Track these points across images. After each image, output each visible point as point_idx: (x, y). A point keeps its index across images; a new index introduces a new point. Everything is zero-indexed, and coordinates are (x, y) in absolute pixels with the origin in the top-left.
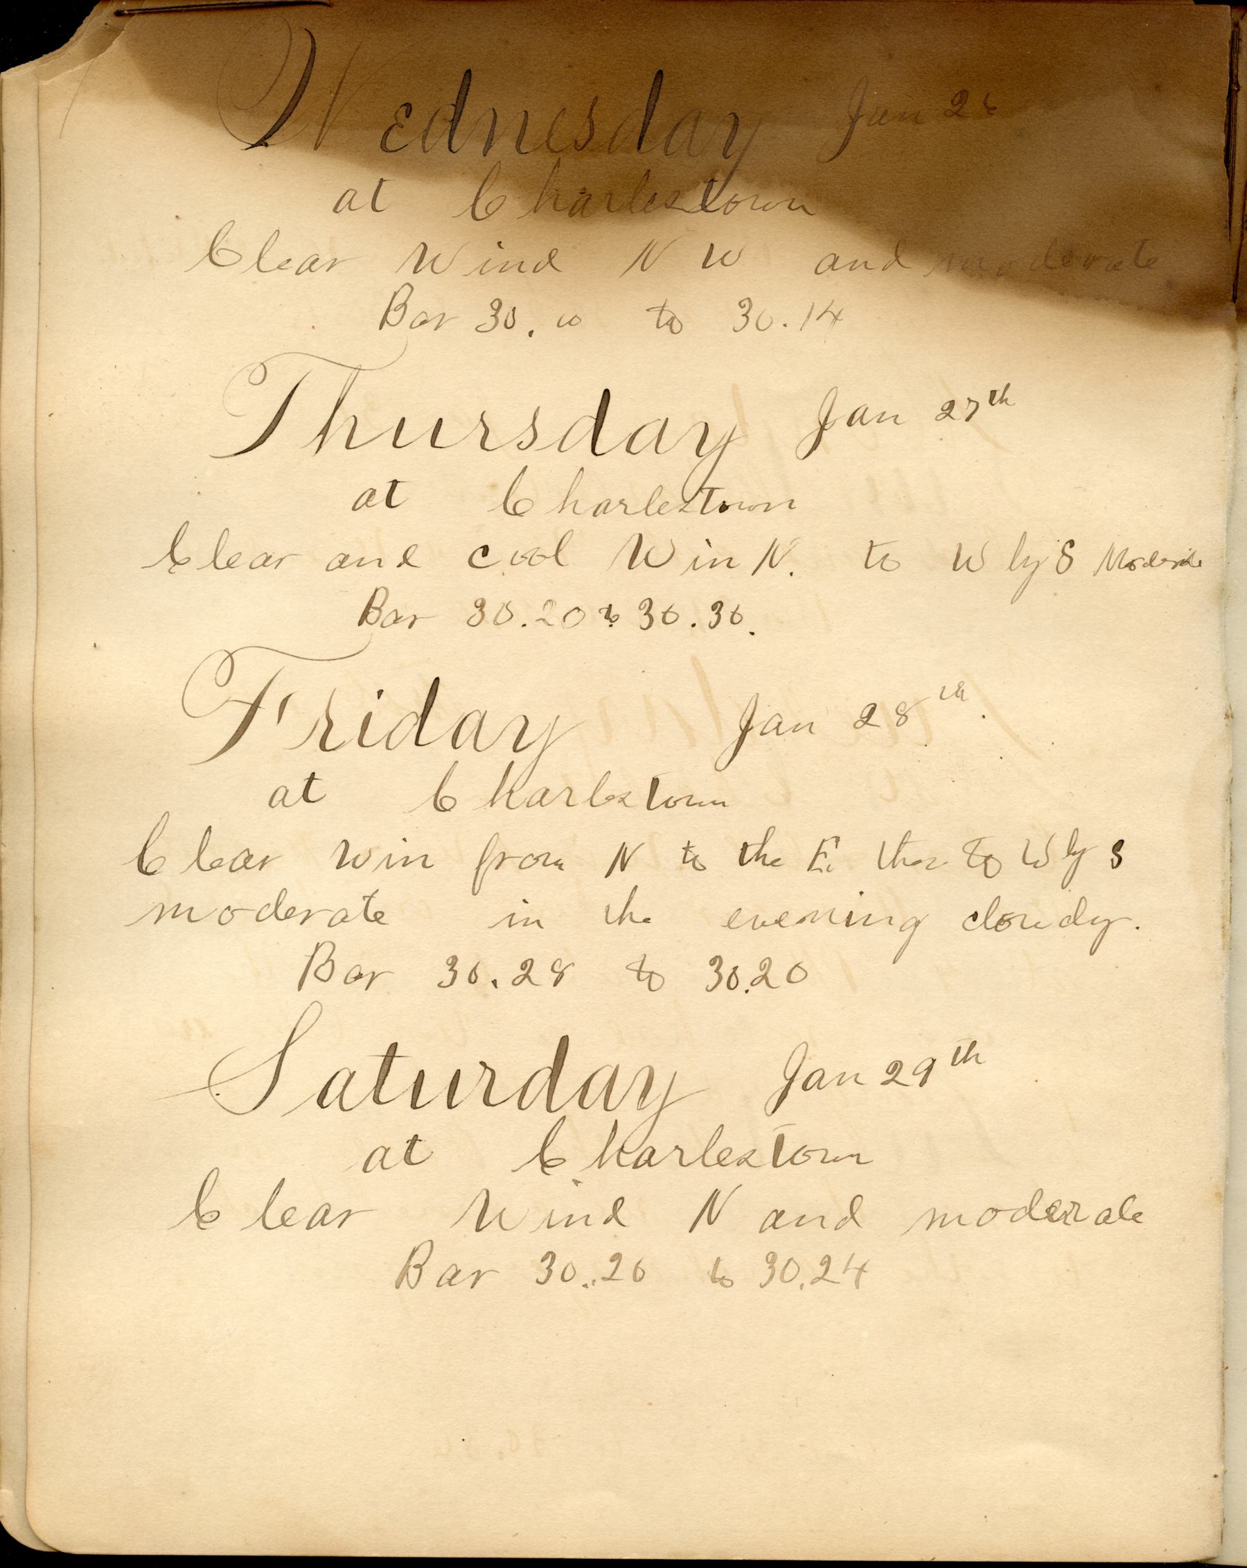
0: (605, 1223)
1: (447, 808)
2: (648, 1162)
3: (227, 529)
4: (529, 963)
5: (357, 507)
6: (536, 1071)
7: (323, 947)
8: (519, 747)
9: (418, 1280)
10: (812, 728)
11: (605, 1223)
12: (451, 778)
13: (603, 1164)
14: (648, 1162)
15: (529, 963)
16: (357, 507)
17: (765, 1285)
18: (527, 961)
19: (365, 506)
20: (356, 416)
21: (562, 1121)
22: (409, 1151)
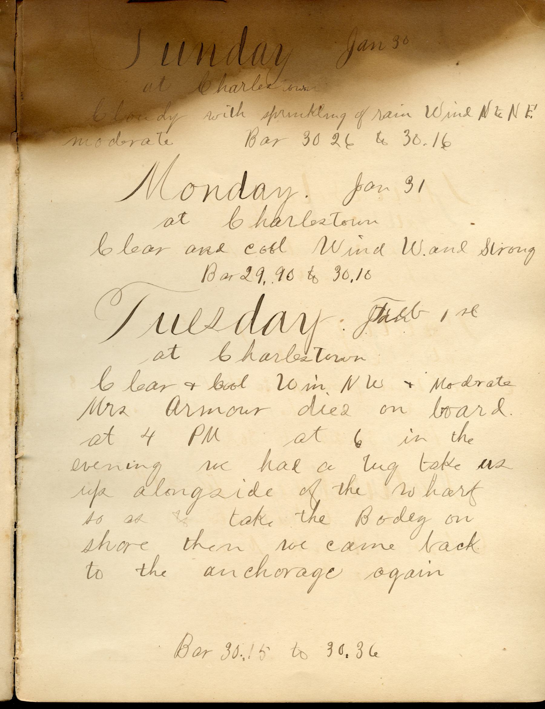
0: (270, 449)
1: (103, 254)
2: (388, 116)
3: (107, 233)
4: (337, 135)
5: (363, 549)
6: (370, 647)
7: (410, 249)
8: (279, 196)
9: (260, 185)
10: (453, 250)
11: (270, 449)
12: (468, 424)
13: (204, 414)
14: (388, 116)
15: (337, 135)
16: (363, 549)
17: (406, 145)
18: (335, 134)
19: (372, 468)
20: (371, 376)
21: (289, 355)
22: (245, 174)
